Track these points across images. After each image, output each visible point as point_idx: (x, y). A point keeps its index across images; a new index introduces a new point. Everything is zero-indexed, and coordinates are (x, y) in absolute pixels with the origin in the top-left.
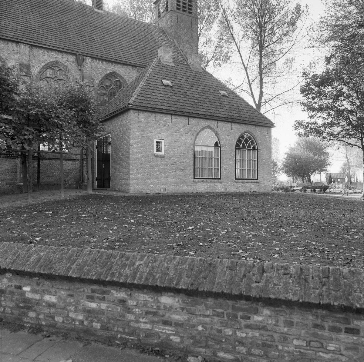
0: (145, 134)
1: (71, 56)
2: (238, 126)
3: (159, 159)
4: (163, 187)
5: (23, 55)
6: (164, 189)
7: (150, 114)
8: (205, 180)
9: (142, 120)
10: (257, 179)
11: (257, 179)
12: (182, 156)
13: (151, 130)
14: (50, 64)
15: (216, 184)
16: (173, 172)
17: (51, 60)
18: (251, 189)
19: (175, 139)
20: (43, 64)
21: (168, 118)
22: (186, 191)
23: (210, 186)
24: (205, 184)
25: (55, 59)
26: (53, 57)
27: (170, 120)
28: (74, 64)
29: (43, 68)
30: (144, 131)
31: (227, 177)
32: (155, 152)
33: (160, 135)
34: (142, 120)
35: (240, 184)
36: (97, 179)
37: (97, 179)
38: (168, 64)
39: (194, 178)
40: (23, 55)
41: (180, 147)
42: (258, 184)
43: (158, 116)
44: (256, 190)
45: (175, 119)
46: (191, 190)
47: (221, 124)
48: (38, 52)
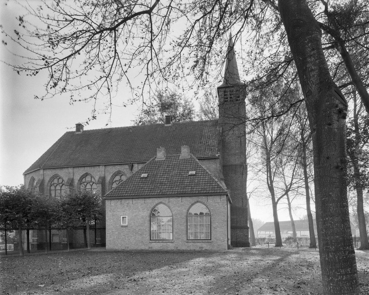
0: (115, 213)
1: (127, 165)
2: (188, 199)
3: (124, 228)
4: (127, 246)
5: (102, 172)
6: (128, 247)
7: (118, 200)
8: (158, 241)
9: (113, 204)
10: (211, 240)
11: (211, 240)
12: (140, 225)
13: (119, 210)
14: (116, 173)
15: (168, 244)
16: (133, 236)
17: (116, 171)
18: (202, 248)
19: (135, 214)
20: (112, 174)
21: (130, 201)
22: (143, 249)
23: (163, 245)
24: (158, 244)
25: (118, 170)
26: (117, 168)
27: (131, 202)
28: (128, 170)
29: (112, 176)
30: (114, 212)
31: (178, 239)
32: (122, 224)
33: (125, 213)
34: (113, 204)
35: (190, 244)
36: (248, 228)
37: (248, 228)
38: (161, 160)
39: (151, 240)
40: (102, 172)
41: (138, 219)
42: (210, 244)
43: (123, 201)
44: (207, 248)
45: (135, 201)
46: (147, 248)
47: (172, 199)
48: (109, 168)
